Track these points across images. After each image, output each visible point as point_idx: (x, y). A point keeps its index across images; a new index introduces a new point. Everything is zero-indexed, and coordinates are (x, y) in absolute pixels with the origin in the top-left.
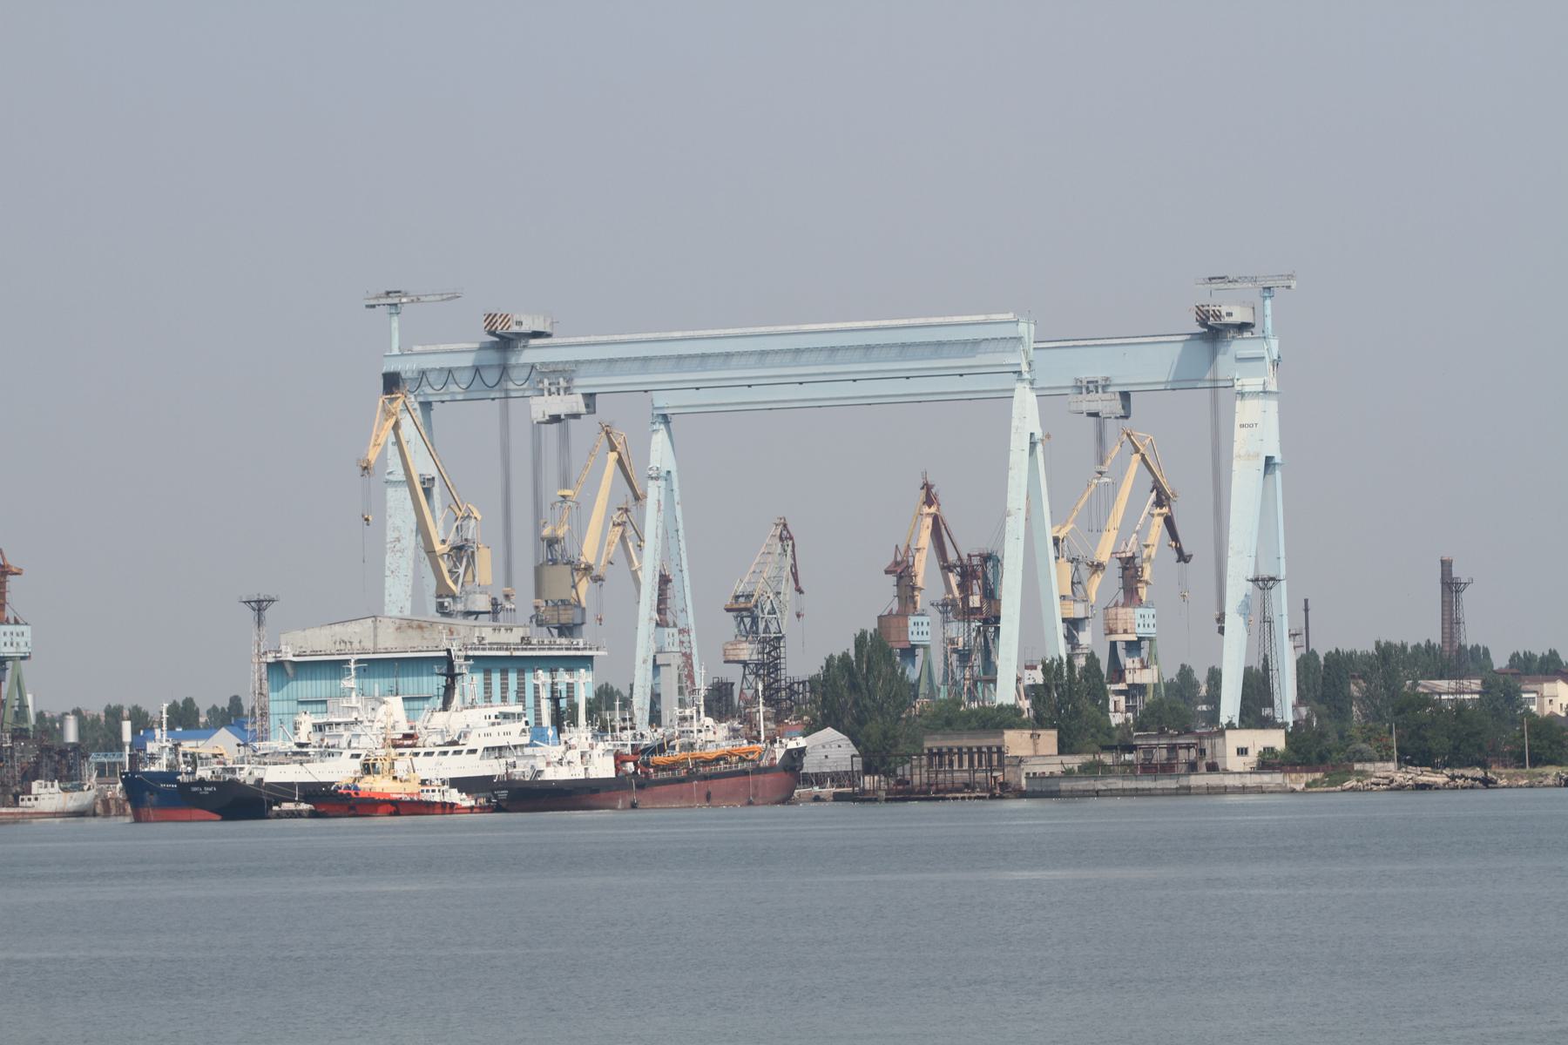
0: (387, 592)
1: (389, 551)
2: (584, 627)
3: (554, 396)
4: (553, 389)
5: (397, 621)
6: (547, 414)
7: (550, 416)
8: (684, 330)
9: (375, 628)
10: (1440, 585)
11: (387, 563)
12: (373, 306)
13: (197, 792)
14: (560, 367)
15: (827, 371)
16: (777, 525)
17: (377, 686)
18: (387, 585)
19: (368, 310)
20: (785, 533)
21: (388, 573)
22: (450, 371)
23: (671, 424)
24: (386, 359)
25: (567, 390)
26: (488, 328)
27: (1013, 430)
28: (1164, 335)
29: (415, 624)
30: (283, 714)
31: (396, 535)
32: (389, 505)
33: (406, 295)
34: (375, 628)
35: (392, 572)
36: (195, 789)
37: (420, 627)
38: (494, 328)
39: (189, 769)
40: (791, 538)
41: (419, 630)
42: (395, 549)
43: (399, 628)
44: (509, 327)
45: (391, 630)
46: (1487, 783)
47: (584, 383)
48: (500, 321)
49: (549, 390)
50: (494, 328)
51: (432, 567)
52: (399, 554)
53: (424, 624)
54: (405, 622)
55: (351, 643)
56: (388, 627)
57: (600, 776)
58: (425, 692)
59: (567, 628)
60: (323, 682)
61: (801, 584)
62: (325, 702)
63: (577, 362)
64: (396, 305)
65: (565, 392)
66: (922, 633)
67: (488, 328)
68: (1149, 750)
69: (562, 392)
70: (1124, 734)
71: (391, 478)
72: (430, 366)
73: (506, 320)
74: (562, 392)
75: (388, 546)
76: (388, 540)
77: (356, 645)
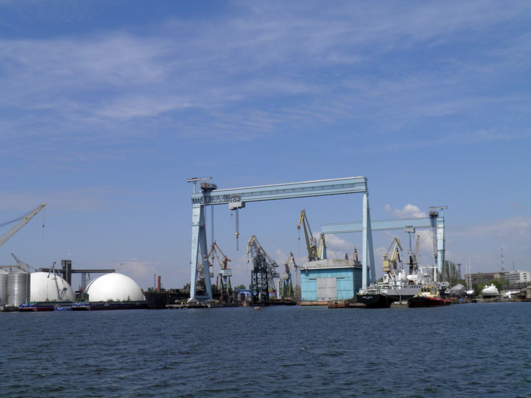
0: (192, 253)
3: (235, 202)
4: (235, 201)
5: (333, 260)
6: (233, 207)
7: (234, 208)
8: (343, 178)
9: (328, 261)
11: (192, 246)
12: (189, 182)
13: (365, 299)
14: (236, 195)
15: (337, 191)
17: (329, 276)
18: (192, 251)
19: (188, 183)
21: (192, 248)
22: (218, 196)
24: (193, 195)
25: (238, 201)
27: (363, 207)
29: (338, 260)
30: (309, 282)
31: (194, 238)
32: (193, 231)
33: (198, 179)
34: (328, 261)
35: (193, 248)
36: (364, 297)
37: (339, 261)
39: (224, 290)
41: (339, 262)
43: (334, 261)
45: (332, 262)
46: (260, 371)
47: (243, 199)
49: (234, 201)
52: (195, 243)
53: (340, 260)
54: (335, 260)
55: (321, 265)
56: (331, 261)
57: (143, 310)
58: (342, 276)
60: (315, 274)
62: (316, 279)
63: (243, 194)
64: (195, 181)
65: (238, 201)
66: (524, 276)
69: (237, 201)
70: (514, 328)
71: (193, 224)
72: (220, 194)
74: (237, 201)
75: (193, 241)
77: (322, 265)
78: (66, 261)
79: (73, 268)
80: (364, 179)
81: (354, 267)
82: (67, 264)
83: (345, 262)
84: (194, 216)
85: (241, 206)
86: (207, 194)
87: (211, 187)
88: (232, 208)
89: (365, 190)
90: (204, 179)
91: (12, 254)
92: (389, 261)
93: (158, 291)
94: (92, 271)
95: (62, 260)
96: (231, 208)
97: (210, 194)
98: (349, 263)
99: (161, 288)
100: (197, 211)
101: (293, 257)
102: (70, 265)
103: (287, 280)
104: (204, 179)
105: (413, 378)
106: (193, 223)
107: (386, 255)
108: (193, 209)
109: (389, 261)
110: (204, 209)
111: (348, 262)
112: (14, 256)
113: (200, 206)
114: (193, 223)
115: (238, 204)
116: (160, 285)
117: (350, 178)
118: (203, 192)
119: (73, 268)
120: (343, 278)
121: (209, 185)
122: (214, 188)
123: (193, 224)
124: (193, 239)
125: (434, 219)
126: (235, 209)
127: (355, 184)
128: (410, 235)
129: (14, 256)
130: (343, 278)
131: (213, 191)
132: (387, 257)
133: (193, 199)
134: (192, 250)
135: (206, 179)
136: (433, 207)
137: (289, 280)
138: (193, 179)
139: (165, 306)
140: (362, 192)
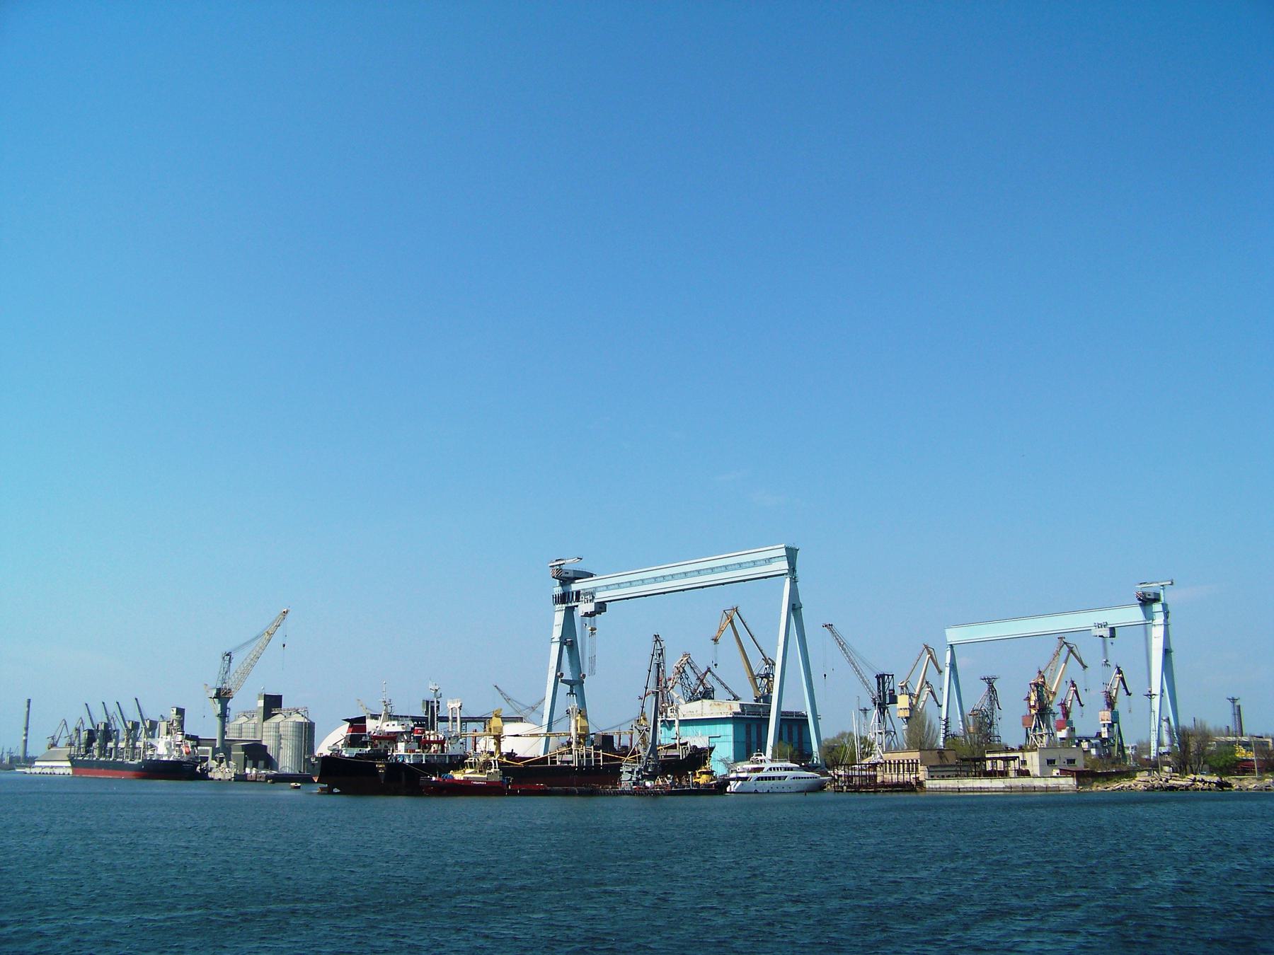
14: (588, 591)
47: (600, 597)
71: (553, 640)
78: (428, 702)
81: (731, 716)
87: (571, 575)
89: (787, 571)
91: (136, 699)
92: (910, 696)
95: (424, 701)
97: (571, 589)
100: (559, 617)
101: (1121, 675)
103: (1111, 726)
104: (569, 561)
105: (1067, 942)
107: (903, 682)
109: (910, 695)
110: (574, 613)
112: (497, 688)
113: (564, 608)
115: (590, 607)
118: (562, 585)
120: (719, 737)
123: (553, 640)
124: (551, 666)
125: (1147, 607)
127: (773, 560)
128: (1104, 642)
129: (497, 688)
130: (719, 737)
131: (577, 581)
132: (906, 686)
136: (1145, 583)
137: (1115, 724)
138: (557, 561)
140: (783, 574)
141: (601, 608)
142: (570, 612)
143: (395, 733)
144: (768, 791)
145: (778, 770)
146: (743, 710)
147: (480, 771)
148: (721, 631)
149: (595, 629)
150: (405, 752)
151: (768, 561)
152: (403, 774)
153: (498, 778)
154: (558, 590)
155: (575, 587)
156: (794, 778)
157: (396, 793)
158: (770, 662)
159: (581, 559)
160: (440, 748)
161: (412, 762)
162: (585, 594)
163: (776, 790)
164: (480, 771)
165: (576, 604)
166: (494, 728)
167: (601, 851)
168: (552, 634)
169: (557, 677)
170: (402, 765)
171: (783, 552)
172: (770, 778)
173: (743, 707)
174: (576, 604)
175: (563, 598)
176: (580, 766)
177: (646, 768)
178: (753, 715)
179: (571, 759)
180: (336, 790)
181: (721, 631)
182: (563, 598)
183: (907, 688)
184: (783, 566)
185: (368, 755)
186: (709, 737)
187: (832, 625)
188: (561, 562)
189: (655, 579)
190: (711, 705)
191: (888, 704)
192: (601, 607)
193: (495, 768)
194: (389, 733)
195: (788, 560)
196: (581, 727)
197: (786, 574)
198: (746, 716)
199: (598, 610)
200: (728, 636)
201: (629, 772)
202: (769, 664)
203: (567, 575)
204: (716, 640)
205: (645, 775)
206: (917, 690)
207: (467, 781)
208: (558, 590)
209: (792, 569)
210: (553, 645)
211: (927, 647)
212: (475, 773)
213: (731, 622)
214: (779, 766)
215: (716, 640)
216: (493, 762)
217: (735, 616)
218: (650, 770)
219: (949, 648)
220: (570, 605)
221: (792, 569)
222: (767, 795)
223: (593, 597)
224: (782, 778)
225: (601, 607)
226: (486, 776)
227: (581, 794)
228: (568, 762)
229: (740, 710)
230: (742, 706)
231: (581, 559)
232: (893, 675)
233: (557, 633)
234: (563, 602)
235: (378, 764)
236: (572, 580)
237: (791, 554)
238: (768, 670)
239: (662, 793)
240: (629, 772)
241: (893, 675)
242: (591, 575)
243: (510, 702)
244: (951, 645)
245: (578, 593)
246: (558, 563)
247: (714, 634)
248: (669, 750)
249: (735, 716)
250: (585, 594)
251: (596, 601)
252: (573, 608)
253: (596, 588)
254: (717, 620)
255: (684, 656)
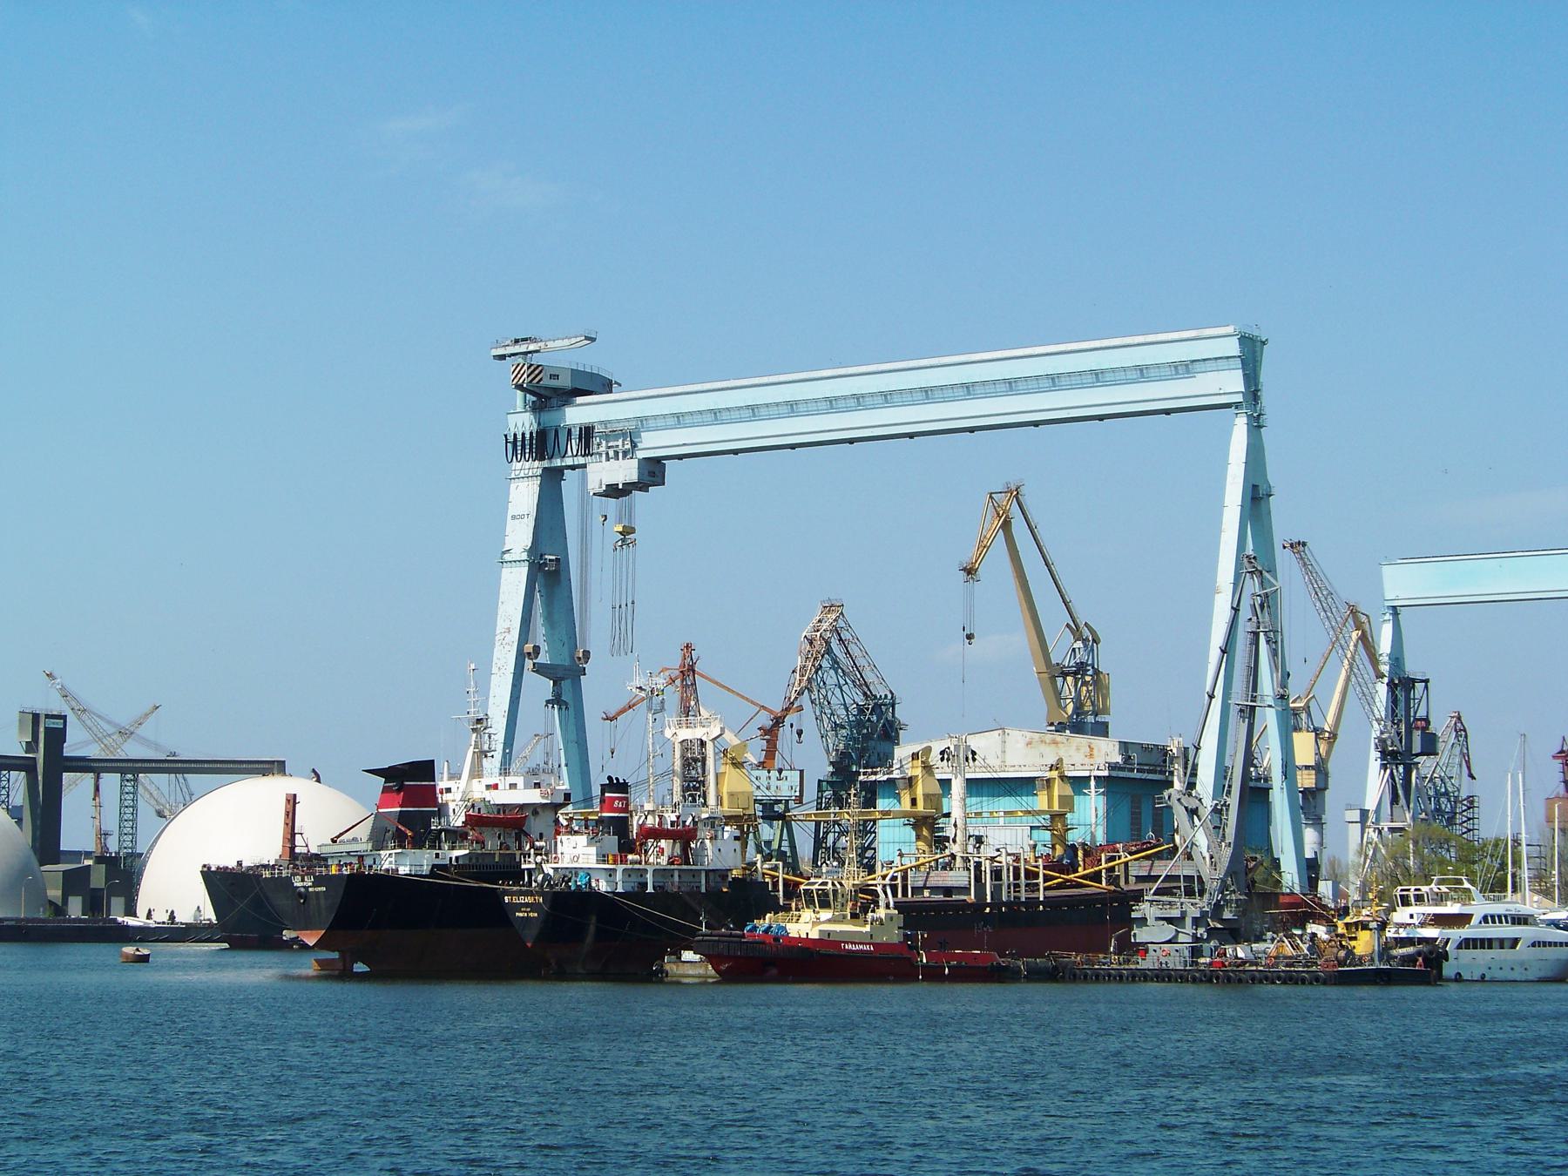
1: (497, 644)
2: (1327, 792)
4: (611, 453)
10: (521, 803)
12: (502, 357)
14: (619, 426)
16: (1452, 717)
20: (1459, 725)
21: (495, 670)
23: (1400, 616)
26: (516, 381)
28: (1139, 345)
38: (521, 381)
40: (1465, 730)
42: (504, 642)
44: (541, 379)
47: (653, 443)
48: (525, 376)
50: (521, 381)
51: (1253, 729)
59: (1309, 791)
61: (1473, 772)
67: (516, 381)
68: (73, 1050)
71: (507, 557)
73: (537, 372)
76: (498, 632)
78: (36, 717)
79: (69, 750)
80: (1234, 342)
81: (1106, 773)
82: (42, 729)
83: (1078, 749)
84: (514, 517)
85: (634, 477)
86: (549, 418)
87: (565, 382)
88: (601, 490)
89: (1239, 398)
90: (559, 343)
93: (238, 870)
94: (109, 765)
96: (597, 490)
97: (563, 418)
98: (1095, 752)
99: (297, 850)
100: (524, 495)
102: (56, 737)
104: (559, 343)
106: (504, 553)
108: (513, 486)
111: (1091, 749)
113: (540, 472)
114: (504, 553)
115: (626, 471)
116: (293, 834)
117: (1097, 344)
119: (69, 750)
121: (554, 377)
122: (594, 384)
123: (507, 557)
124: (501, 625)
126: (613, 491)
127: (1197, 366)
131: (579, 400)
133: (511, 439)
134: (494, 680)
135: (566, 342)
138: (517, 341)
139: (1130, 915)
141: (652, 474)
142: (552, 480)
143: (522, 807)
144: (1483, 976)
145: (1494, 922)
146: (1127, 759)
147: (854, 916)
148: (984, 547)
149: (632, 531)
150: (598, 862)
151: (1185, 368)
152: (594, 919)
153: (893, 935)
154: (523, 422)
155: (576, 414)
156: (1533, 945)
157: (562, 974)
158: (1086, 633)
159: (593, 340)
160: (678, 850)
161: (620, 890)
162: (607, 437)
163: (1500, 975)
164: (854, 916)
165: (581, 460)
166: (731, 795)
167: (98, 1103)
168: (502, 535)
169: (521, 656)
170: (594, 896)
171: (1232, 347)
172: (1486, 943)
173: (1127, 751)
174: (581, 460)
175: (541, 444)
176: (996, 903)
177: (1217, 908)
178: (1149, 772)
179: (964, 883)
180: (360, 967)
181: (984, 547)
182: (541, 444)
183: (1309, 715)
184: (1232, 383)
185: (461, 868)
186: (1032, 828)
187: (1304, 544)
188: (532, 347)
189: (832, 404)
190: (1029, 744)
191: (1417, 755)
192: (653, 472)
193: (888, 906)
194: (504, 807)
195: (1244, 369)
196: (731, 795)
197: (1237, 405)
198: (1135, 774)
199: (647, 479)
200: (997, 563)
201: (1170, 920)
202: (1085, 641)
203: (554, 383)
204: (970, 571)
205: (1216, 928)
206: (1330, 718)
207: (827, 941)
208: (523, 422)
209: (1253, 393)
210: (506, 572)
211: (1354, 612)
212: (842, 920)
213: (1006, 526)
214: (1502, 912)
215: (970, 571)
216: (879, 889)
217: (1015, 510)
218: (1227, 915)
219: (1388, 617)
220: (557, 462)
221: (1253, 393)
222: (1478, 986)
223: (634, 445)
224: (1506, 944)
225: (653, 472)
226: (868, 928)
227: (1036, 975)
228: (948, 891)
229: (1119, 759)
230: (1125, 747)
231: (593, 340)
232: (1426, 681)
233: (519, 537)
234: (540, 457)
235: (512, 894)
236: (570, 395)
237: (1251, 353)
238: (1082, 656)
239: (1121, 976)
240: (1170, 920)
241: (1426, 681)
242: (607, 386)
243: (84, 717)
244: (1394, 608)
245: (587, 433)
246: (522, 348)
247: (968, 555)
248: (1157, 863)
249: (1114, 774)
250: (607, 437)
251: (641, 455)
252: (559, 472)
253: (642, 420)
254: (977, 520)
255: (829, 608)
